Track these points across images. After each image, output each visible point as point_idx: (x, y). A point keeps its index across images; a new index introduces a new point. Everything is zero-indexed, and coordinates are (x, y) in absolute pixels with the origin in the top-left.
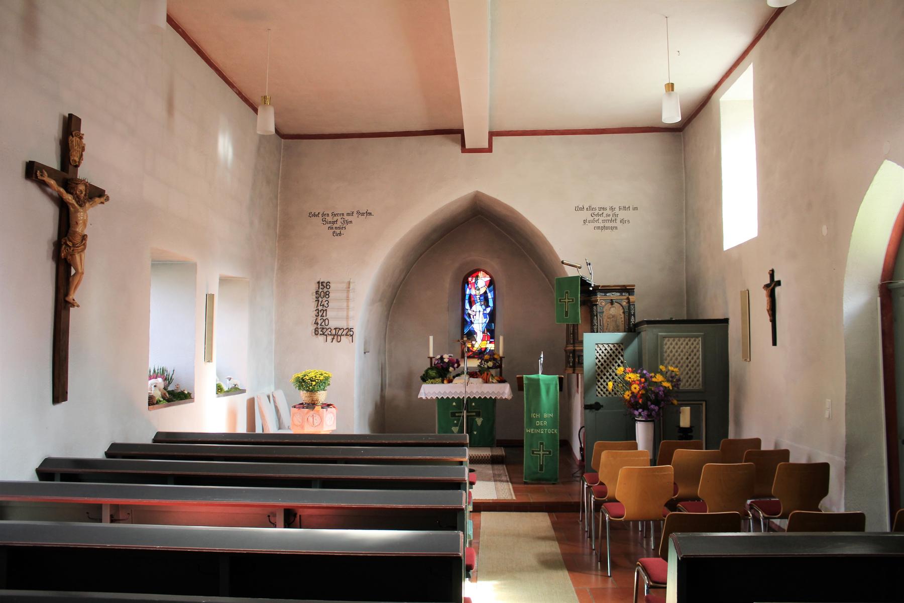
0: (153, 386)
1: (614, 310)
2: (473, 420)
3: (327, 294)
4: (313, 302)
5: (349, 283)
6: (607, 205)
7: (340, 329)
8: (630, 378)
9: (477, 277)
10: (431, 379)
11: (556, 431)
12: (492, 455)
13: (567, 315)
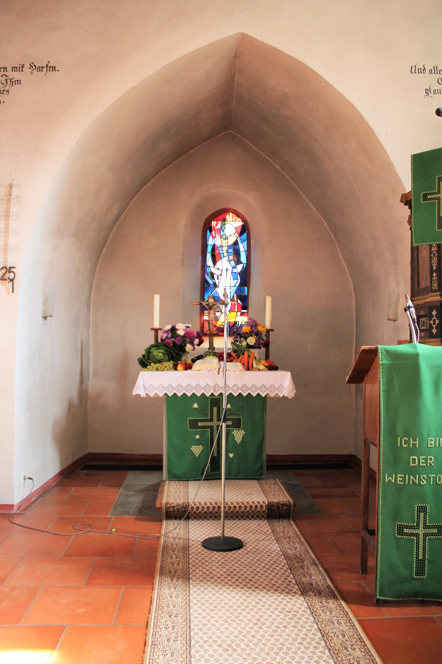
5: (11, 186)
9: (224, 220)
10: (155, 363)
12: (269, 504)
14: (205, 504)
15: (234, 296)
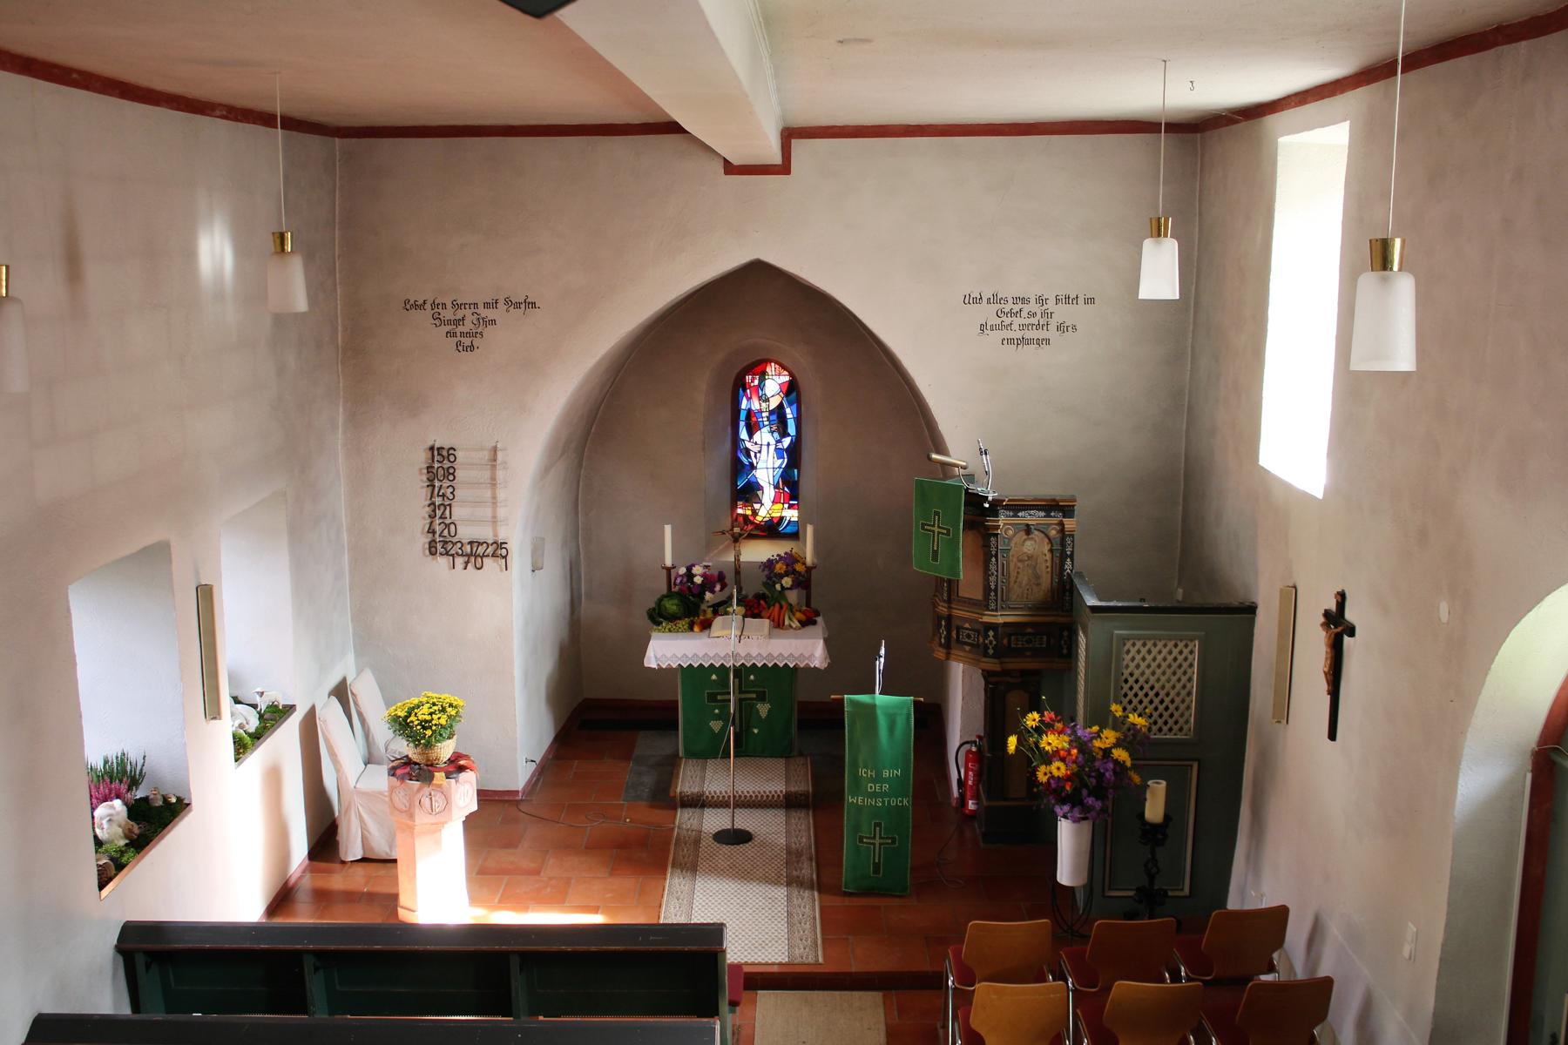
0: (104, 822)
1: (1032, 545)
2: (752, 707)
3: (450, 473)
4: (422, 487)
5: (495, 450)
6: (1032, 294)
7: (480, 544)
8: (1049, 744)
11: (905, 802)
13: (935, 558)
14: (721, 792)
15: (778, 482)
